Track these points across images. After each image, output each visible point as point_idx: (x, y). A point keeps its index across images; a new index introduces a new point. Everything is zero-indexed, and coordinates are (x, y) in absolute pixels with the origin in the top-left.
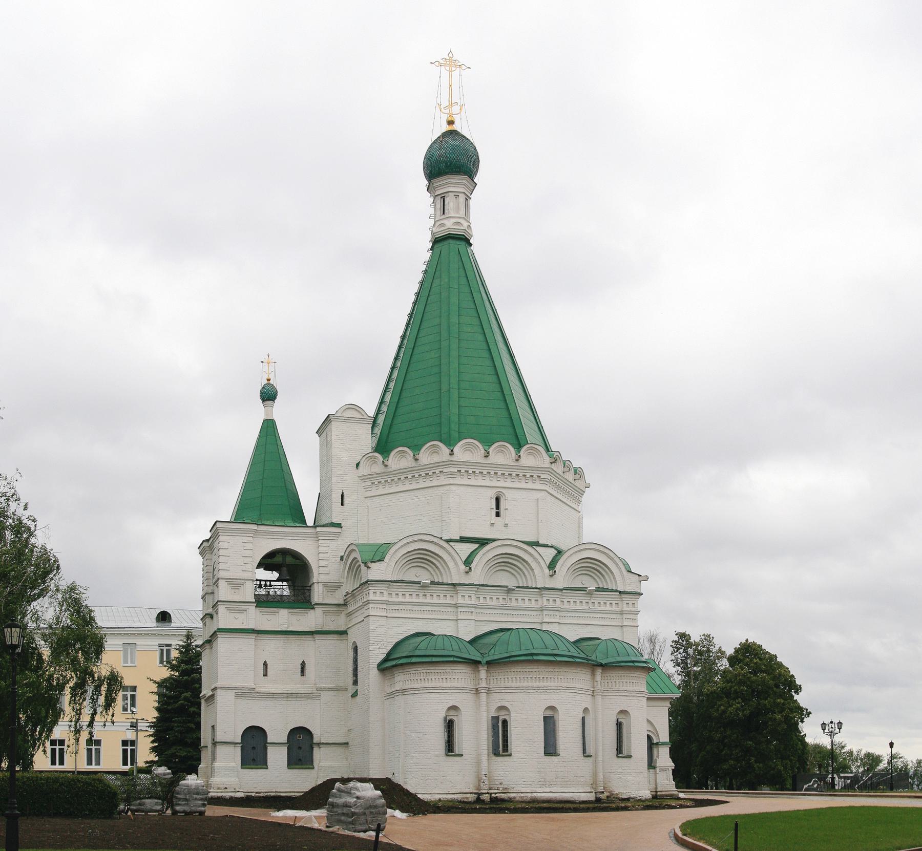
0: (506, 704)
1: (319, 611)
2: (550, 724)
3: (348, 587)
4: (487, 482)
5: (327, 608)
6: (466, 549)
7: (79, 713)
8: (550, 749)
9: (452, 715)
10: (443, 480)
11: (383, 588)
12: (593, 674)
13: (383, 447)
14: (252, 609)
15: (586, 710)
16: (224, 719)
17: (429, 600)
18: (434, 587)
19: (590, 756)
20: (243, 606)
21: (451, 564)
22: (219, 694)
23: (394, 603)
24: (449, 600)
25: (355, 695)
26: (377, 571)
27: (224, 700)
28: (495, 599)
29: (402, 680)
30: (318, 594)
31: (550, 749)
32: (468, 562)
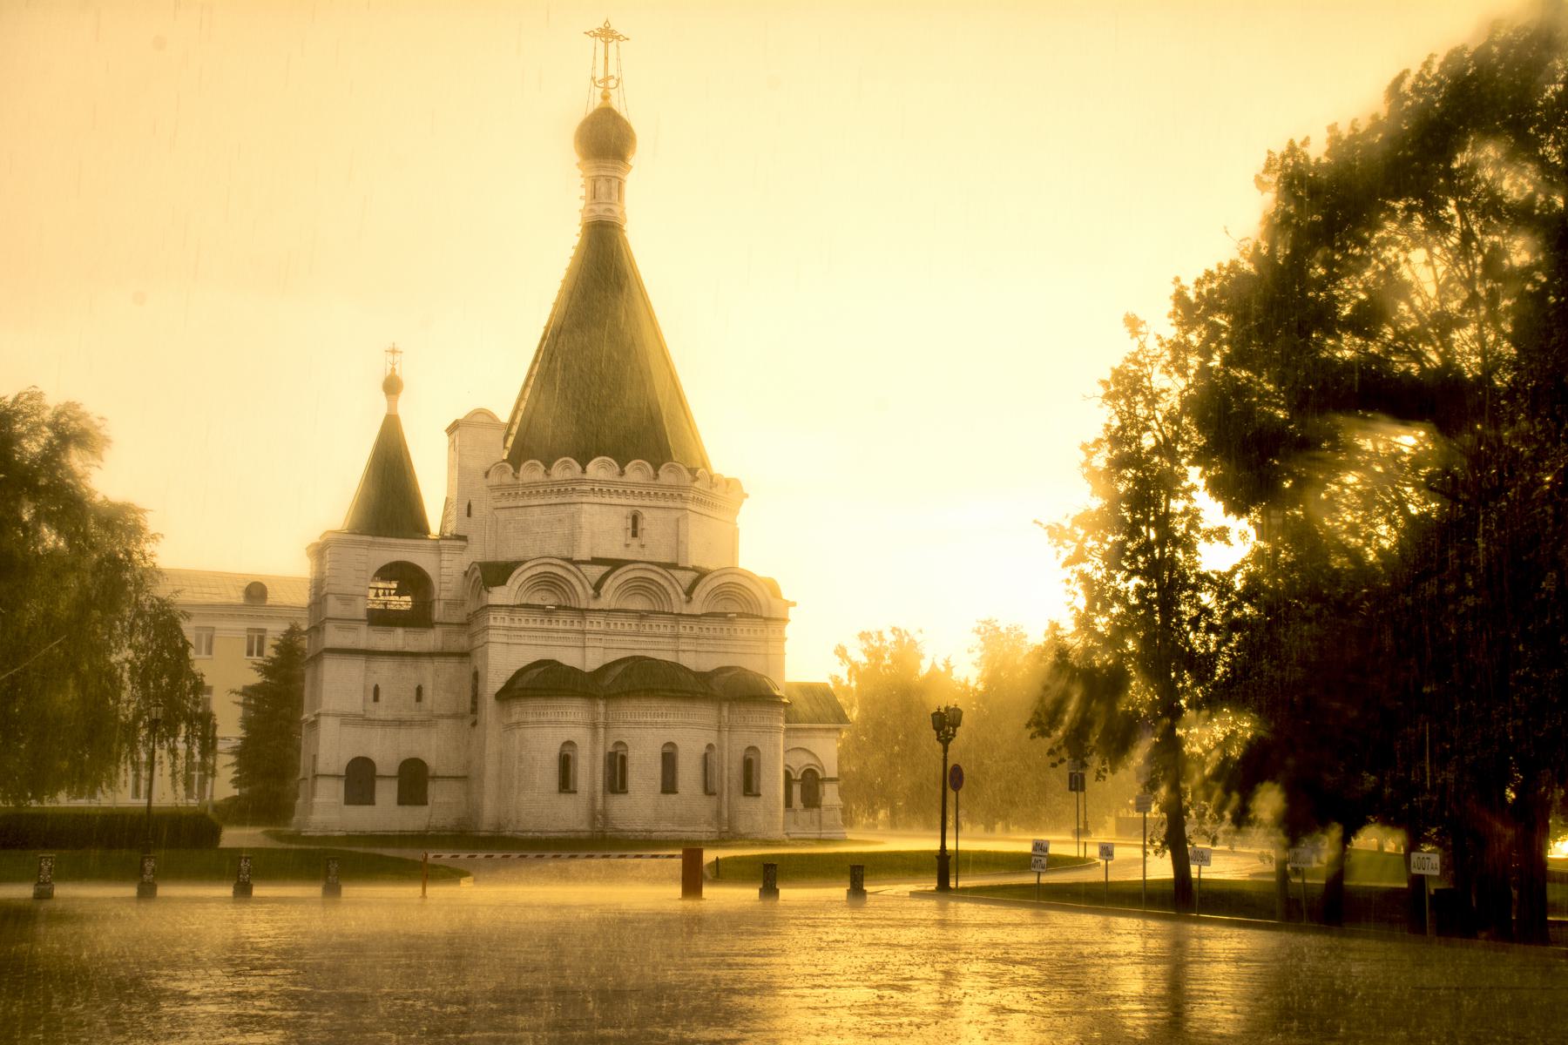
0: (625, 740)
1: (438, 631)
2: (669, 759)
3: (471, 606)
4: (623, 501)
5: (447, 628)
6: (596, 572)
7: (696, 965)
8: (669, 785)
9: (568, 751)
10: (575, 498)
11: (503, 613)
12: (720, 710)
13: (517, 457)
14: (364, 628)
15: (710, 746)
16: (331, 745)
17: (554, 626)
18: (561, 612)
19: (714, 794)
20: (353, 625)
21: (579, 589)
22: (323, 720)
23: (515, 629)
24: (576, 626)
25: (474, 724)
26: (498, 595)
27: (329, 730)
28: (630, 625)
29: (518, 711)
30: (438, 612)
31: (669, 785)
32: (597, 587)
